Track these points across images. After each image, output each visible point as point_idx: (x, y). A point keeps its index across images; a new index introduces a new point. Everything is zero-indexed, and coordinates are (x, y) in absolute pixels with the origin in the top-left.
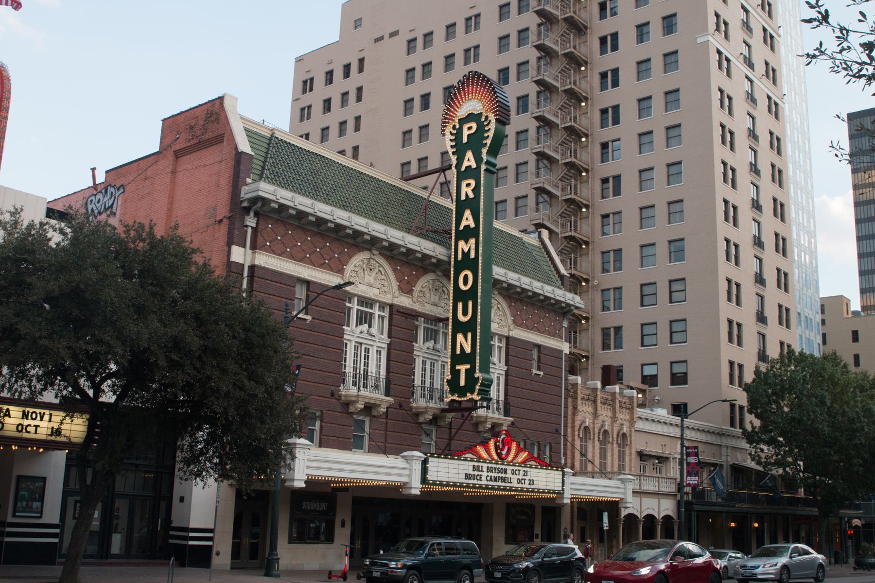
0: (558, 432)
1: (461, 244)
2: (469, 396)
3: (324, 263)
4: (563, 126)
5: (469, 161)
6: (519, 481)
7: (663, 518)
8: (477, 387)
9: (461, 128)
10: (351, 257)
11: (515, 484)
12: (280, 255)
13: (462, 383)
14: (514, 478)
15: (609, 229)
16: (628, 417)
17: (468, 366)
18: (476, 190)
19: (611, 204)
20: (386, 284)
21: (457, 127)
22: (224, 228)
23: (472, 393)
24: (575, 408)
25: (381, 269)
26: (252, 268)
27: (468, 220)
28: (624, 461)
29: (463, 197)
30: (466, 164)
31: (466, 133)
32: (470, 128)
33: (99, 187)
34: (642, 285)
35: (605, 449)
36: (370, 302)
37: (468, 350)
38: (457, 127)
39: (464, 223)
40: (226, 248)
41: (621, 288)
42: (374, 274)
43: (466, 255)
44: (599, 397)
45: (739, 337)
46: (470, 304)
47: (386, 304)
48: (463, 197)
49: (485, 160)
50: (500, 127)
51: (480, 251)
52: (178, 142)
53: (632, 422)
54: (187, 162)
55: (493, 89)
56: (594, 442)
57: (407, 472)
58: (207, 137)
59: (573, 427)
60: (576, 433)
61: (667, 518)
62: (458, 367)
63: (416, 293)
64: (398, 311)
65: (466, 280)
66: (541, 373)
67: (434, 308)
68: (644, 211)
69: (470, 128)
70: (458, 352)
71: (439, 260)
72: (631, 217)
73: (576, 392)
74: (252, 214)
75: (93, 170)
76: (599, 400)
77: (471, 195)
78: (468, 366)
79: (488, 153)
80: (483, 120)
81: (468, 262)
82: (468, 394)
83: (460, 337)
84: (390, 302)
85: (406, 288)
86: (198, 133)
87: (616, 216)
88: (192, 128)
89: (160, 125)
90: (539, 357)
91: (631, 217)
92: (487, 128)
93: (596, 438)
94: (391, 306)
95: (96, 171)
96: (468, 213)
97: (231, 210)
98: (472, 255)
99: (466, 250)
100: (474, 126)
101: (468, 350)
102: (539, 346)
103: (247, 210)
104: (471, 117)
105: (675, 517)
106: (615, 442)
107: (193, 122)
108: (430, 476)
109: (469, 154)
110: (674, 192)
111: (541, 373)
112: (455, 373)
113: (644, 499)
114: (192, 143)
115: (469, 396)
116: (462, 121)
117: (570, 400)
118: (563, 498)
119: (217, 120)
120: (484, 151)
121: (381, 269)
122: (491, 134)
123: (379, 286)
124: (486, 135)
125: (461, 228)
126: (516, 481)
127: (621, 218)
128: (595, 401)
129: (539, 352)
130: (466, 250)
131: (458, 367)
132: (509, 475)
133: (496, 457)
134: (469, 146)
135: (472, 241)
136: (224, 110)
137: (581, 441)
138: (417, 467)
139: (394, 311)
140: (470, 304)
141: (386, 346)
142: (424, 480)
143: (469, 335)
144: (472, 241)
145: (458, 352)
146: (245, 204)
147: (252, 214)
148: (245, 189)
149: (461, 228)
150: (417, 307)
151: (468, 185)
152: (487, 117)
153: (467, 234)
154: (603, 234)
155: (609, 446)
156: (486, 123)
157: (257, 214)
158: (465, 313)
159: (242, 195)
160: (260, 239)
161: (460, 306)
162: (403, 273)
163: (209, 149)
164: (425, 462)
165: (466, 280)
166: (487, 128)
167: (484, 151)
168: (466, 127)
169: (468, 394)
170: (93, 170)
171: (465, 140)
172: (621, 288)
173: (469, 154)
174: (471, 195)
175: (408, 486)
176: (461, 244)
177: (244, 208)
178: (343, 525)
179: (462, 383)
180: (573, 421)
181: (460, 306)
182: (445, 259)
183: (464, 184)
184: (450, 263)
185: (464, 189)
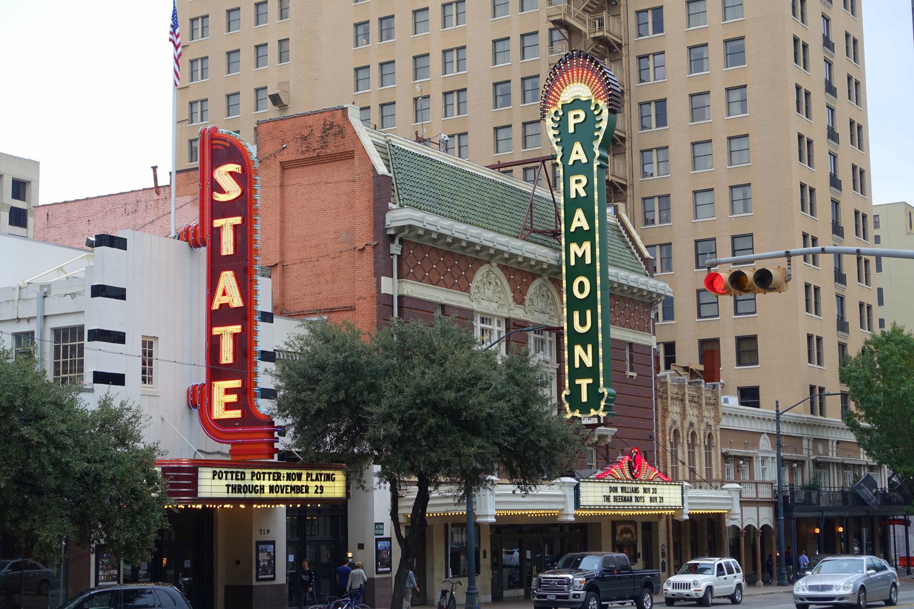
0: (651, 437)
1: (574, 247)
2: (593, 412)
3: (440, 279)
4: (592, 36)
5: (578, 153)
6: (651, 499)
7: (763, 527)
8: (603, 403)
9: (565, 115)
10: (474, 273)
11: (647, 503)
12: (421, 281)
13: (584, 399)
14: (647, 496)
15: (652, 168)
16: (713, 414)
17: (590, 381)
18: (588, 187)
19: (652, 137)
20: (502, 296)
21: (561, 113)
22: (368, 259)
23: (597, 409)
24: (665, 410)
25: (497, 281)
26: (401, 298)
27: (580, 220)
28: (710, 465)
29: (573, 195)
30: (573, 157)
31: (572, 122)
32: (576, 117)
33: (161, 190)
34: (697, 242)
35: (710, 454)
36: (489, 317)
37: (589, 363)
38: (561, 113)
39: (575, 224)
40: (375, 279)
41: (670, 244)
42: (492, 287)
43: (580, 260)
44: (687, 395)
45: (817, 304)
46: (589, 313)
47: (503, 317)
48: (573, 195)
49: (598, 155)
50: (612, 115)
51: (598, 253)
52: (285, 151)
53: (717, 420)
54: (297, 177)
55: (601, 68)
56: (683, 446)
57: (730, 502)
58: (329, 152)
59: (664, 431)
60: (668, 438)
61: (765, 527)
62: (578, 382)
63: (527, 302)
64: (514, 324)
65: (581, 287)
66: (635, 374)
67: (541, 316)
68: (696, 147)
69: (576, 117)
70: (577, 365)
71: (550, 265)
72: (680, 153)
73: (665, 392)
74: (397, 241)
75: (155, 168)
76: (687, 398)
77: (583, 194)
78: (590, 381)
79: (601, 147)
80: (593, 108)
81: (581, 268)
82: (592, 410)
83: (578, 349)
84: (507, 316)
85: (519, 300)
86: (315, 145)
87: (661, 152)
88: (304, 138)
89: (697, 344)
90: (631, 356)
91: (680, 153)
92: (598, 119)
93: (685, 441)
94: (507, 320)
95: (157, 170)
96: (579, 213)
97: (375, 238)
98: (588, 261)
99: (580, 255)
100: (582, 115)
101: (589, 363)
102: (631, 344)
103: (392, 238)
104: (576, 103)
105: (772, 527)
106: (702, 444)
107: (306, 132)
108: (583, 501)
109: (577, 146)
110: (738, 123)
111: (635, 374)
112: (576, 389)
113: (760, 508)
114: (307, 155)
115: (593, 412)
116: (566, 107)
117: (659, 400)
118: (683, 514)
119: (341, 133)
120: (597, 144)
121: (497, 281)
122: (604, 125)
123: (496, 299)
124: (597, 126)
125: (572, 229)
126: (649, 500)
127: (668, 154)
128: (682, 400)
129: (631, 350)
130: (580, 255)
131: (578, 382)
132: (641, 494)
133: (629, 476)
134: (575, 137)
135: (587, 245)
136: (350, 123)
137: (672, 447)
138: (571, 493)
139: (512, 322)
140: (589, 313)
141: (555, 371)
142: (577, 505)
143: (590, 347)
144: (587, 245)
145: (577, 365)
146: (392, 232)
147: (397, 241)
148: (389, 217)
149: (572, 229)
150: (529, 318)
151: (578, 182)
152: (597, 106)
153: (579, 236)
154: (644, 174)
155: (696, 449)
156: (596, 112)
157: (401, 241)
158: (583, 323)
159: (388, 222)
160: (405, 267)
161: (576, 315)
162: (515, 282)
163: (332, 164)
164: (577, 488)
165: (581, 287)
166: (598, 119)
167: (597, 144)
168: (571, 114)
169: (592, 410)
170: (155, 168)
171: (571, 130)
172: (670, 244)
173: (577, 146)
174: (583, 194)
175: (564, 512)
176: (574, 247)
177: (390, 235)
178: (485, 557)
179: (584, 399)
180: (664, 425)
181: (576, 315)
182: (554, 263)
183: (573, 179)
184: (560, 267)
185: (573, 186)
